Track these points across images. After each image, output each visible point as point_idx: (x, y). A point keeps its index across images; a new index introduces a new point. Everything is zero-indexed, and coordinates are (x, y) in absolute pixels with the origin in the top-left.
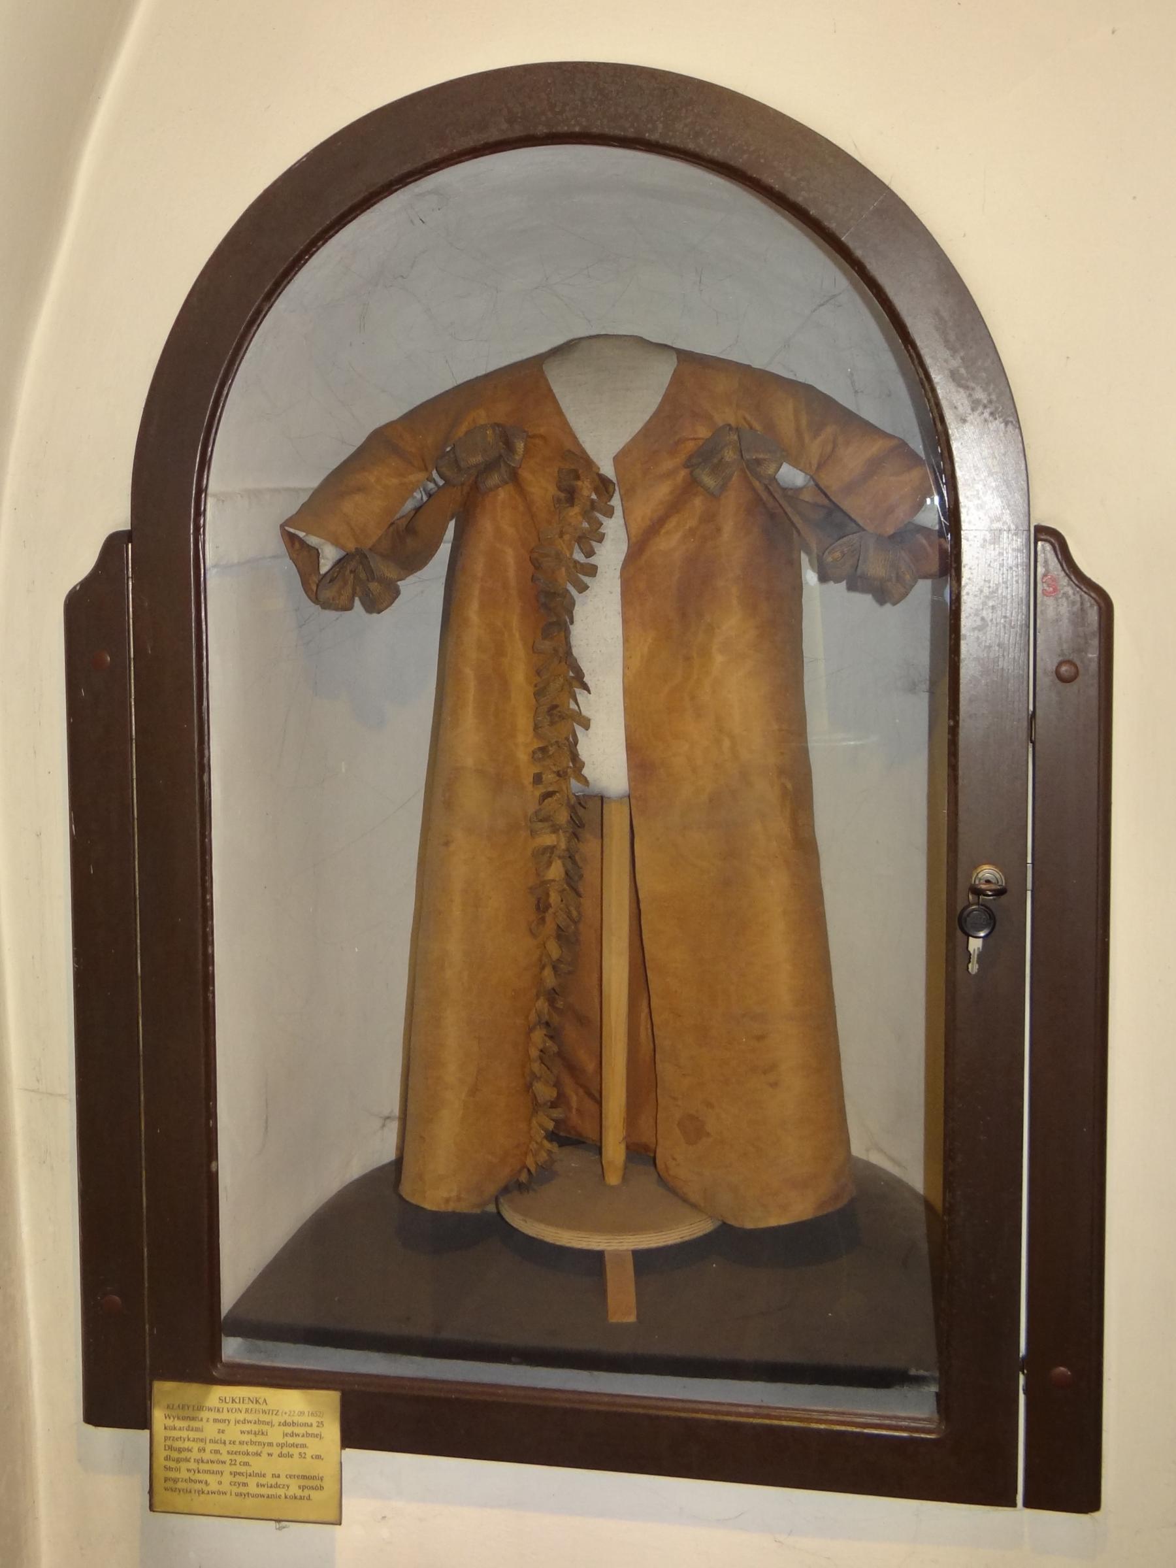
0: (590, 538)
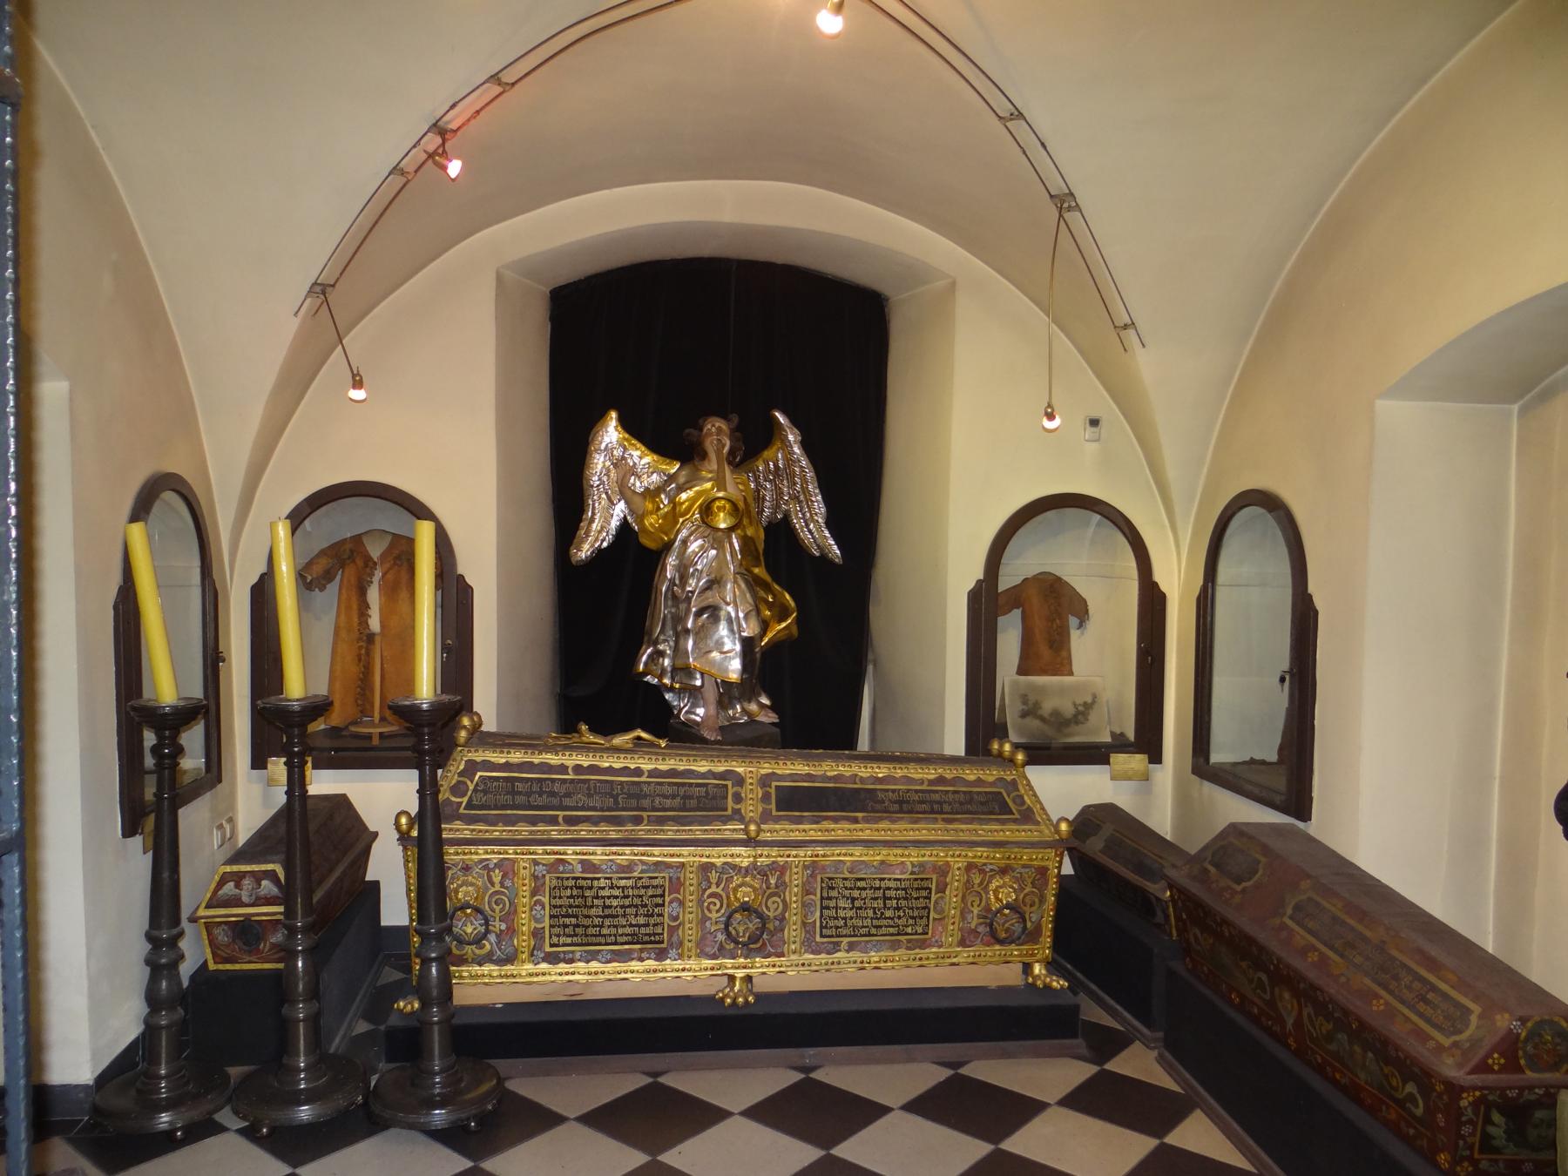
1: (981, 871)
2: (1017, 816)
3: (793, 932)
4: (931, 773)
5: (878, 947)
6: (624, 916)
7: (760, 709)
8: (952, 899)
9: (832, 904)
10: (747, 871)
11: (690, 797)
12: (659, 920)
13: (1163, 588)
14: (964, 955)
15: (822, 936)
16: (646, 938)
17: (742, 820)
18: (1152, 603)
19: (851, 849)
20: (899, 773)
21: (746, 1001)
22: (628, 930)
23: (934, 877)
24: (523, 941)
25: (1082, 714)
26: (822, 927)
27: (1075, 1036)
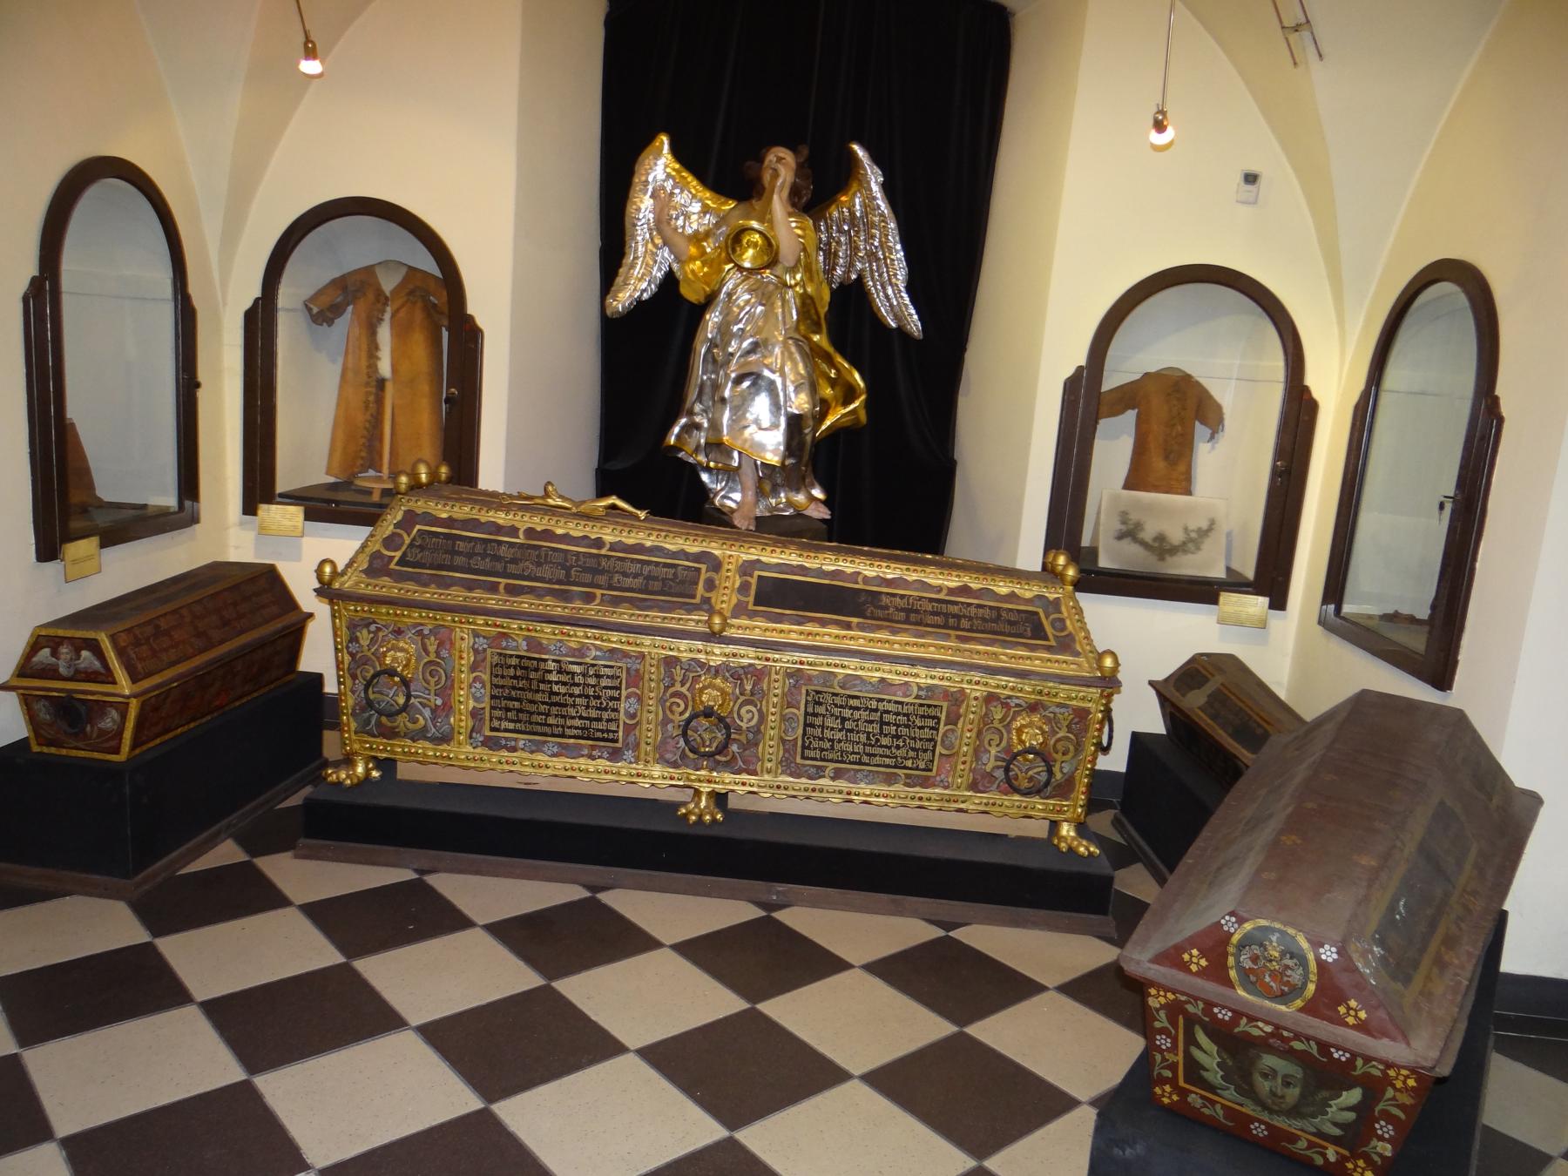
0: (383, 312)
1: (1006, 705)
2: (1053, 643)
3: (770, 748)
4: (953, 582)
5: (871, 778)
6: (574, 706)
7: (812, 500)
8: (965, 735)
9: (818, 721)
10: (717, 671)
11: (655, 579)
12: (613, 715)
13: (1316, 394)
14: (976, 801)
15: (803, 757)
16: (599, 735)
17: (711, 611)
18: (1299, 412)
19: (846, 661)
20: (912, 577)
21: (714, 820)
22: (577, 723)
23: (945, 705)
24: (461, 721)
25: (1195, 540)
26: (804, 747)
27: (1104, 912)
